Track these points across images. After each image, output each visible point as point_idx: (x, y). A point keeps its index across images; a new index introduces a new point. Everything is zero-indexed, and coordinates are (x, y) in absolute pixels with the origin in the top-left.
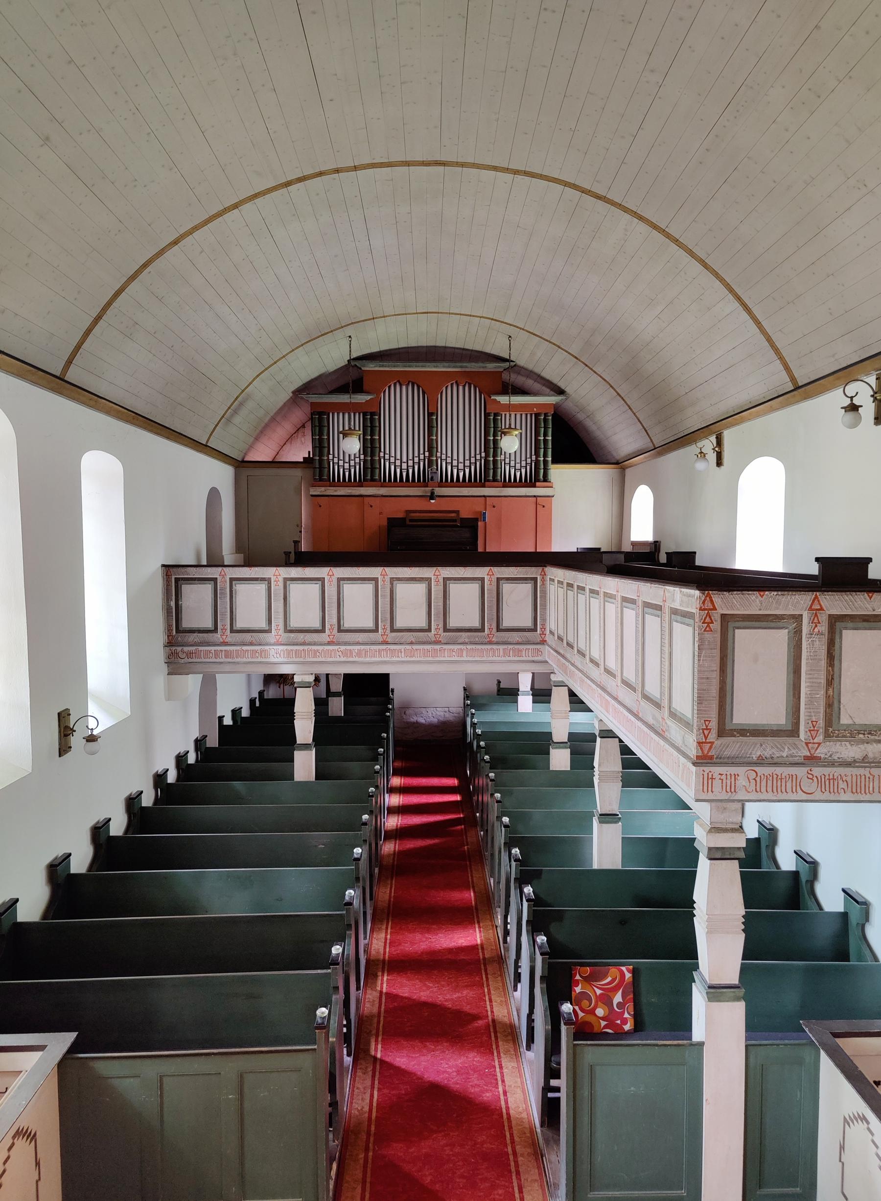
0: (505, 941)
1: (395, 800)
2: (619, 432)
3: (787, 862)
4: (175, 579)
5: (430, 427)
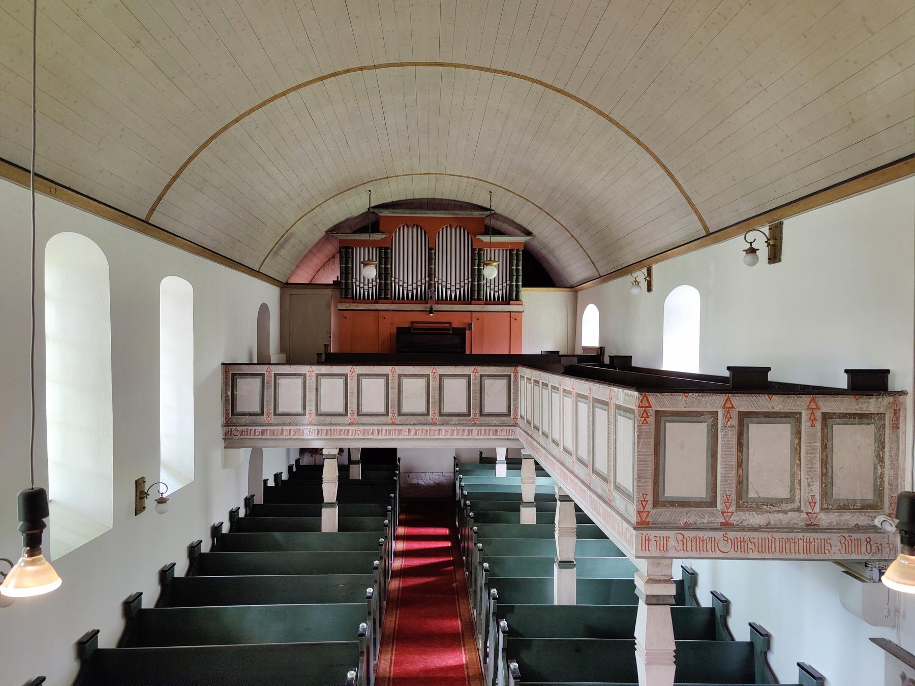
0: (485, 662)
1: (400, 546)
2: (571, 262)
3: (705, 601)
4: (232, 374)
5: (430, 259)
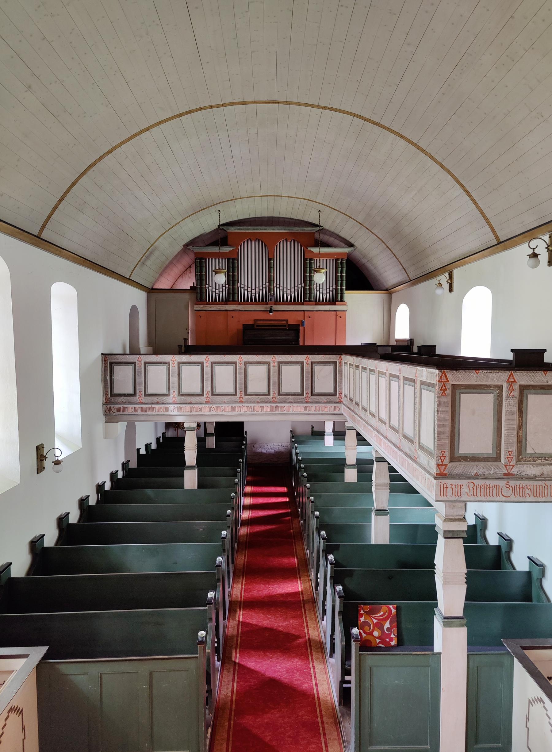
0: (316, 589)
1: (247, 501)
2: (388, 270)
3: (493, 540)
4: (110, 362)
5: (270, 267)
